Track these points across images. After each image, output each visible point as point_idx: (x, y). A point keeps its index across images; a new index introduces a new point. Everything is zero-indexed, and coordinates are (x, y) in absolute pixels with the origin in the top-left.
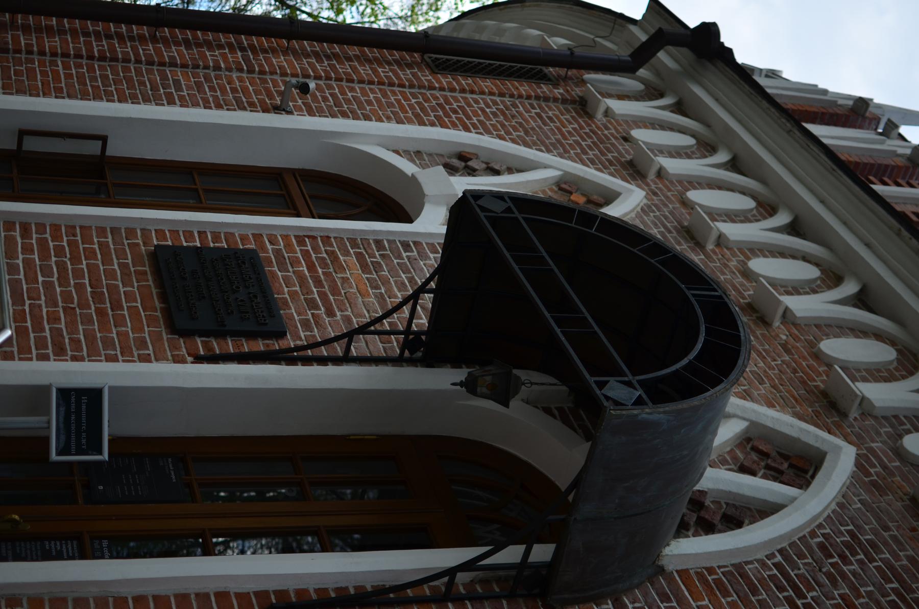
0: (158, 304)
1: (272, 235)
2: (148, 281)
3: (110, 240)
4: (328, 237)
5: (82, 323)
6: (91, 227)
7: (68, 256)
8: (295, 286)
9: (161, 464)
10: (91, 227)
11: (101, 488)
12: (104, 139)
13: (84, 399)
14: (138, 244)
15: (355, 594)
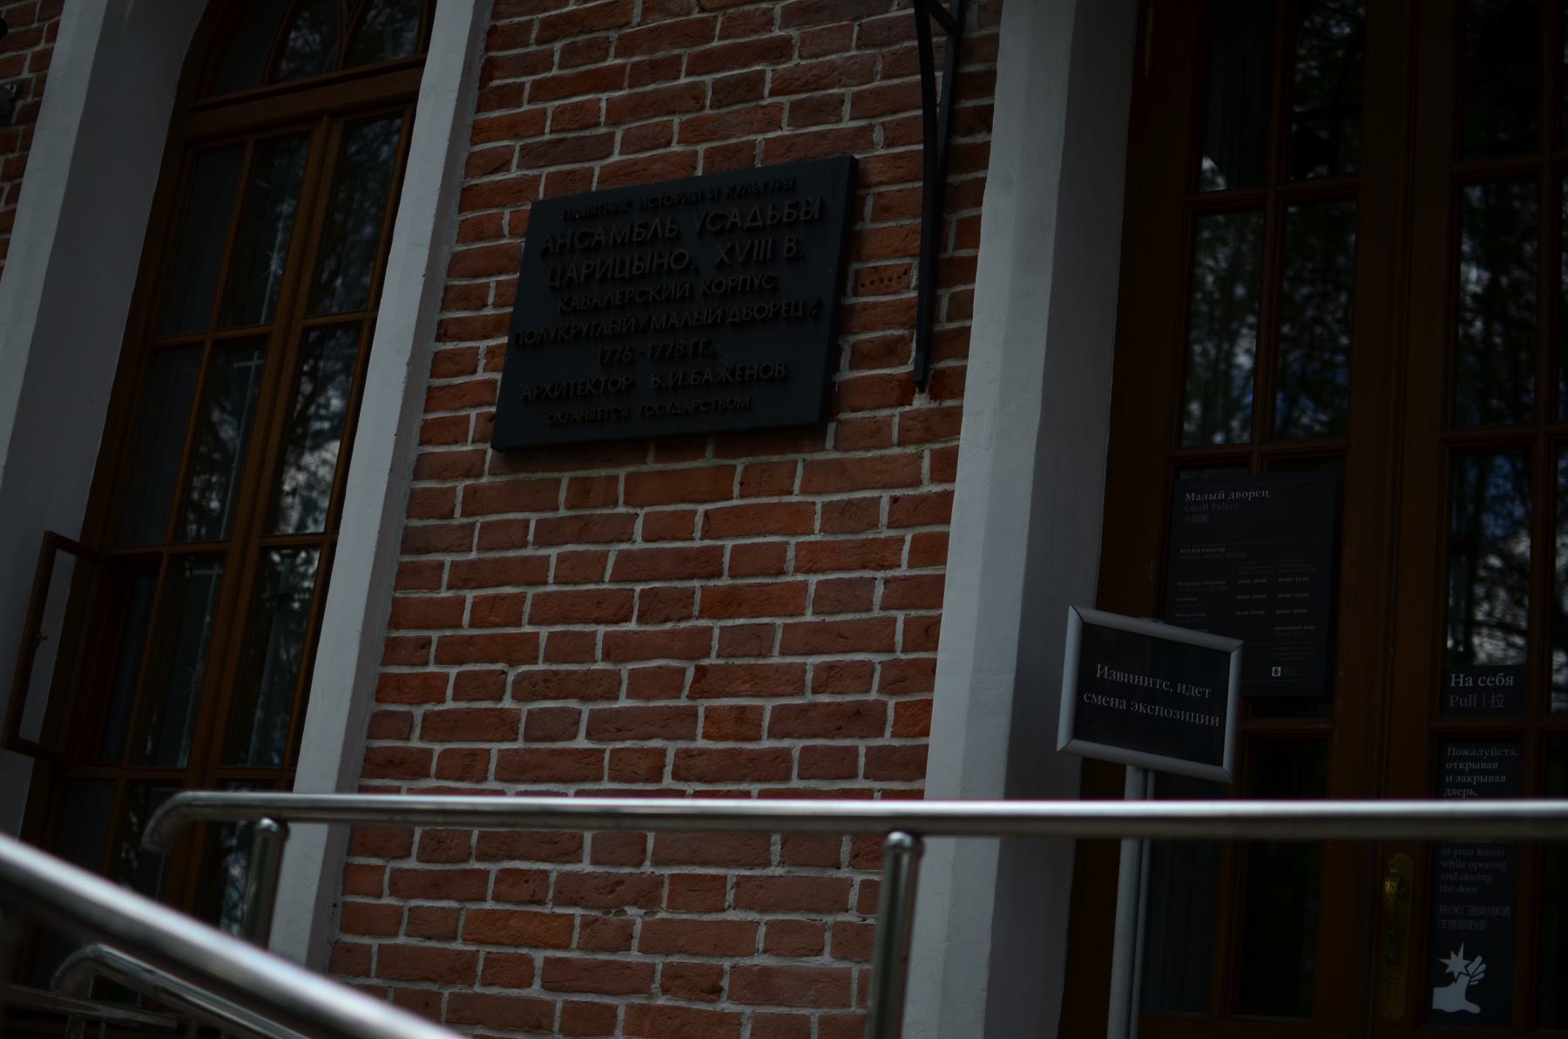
0: (708, 461)
1: (467, 164)
2: (614, 480)
3: (448, 559)
4: (493, 31)
5: (760, 655)
6: (395, 601)
7: (499, 666)
8: (668, 125)
9: (1204, 518)
10: (395, 601)
11: (1277, 671)
12: (54, 542)
13: (1103, 671)
14: (470, 493)
15: (925, 180)
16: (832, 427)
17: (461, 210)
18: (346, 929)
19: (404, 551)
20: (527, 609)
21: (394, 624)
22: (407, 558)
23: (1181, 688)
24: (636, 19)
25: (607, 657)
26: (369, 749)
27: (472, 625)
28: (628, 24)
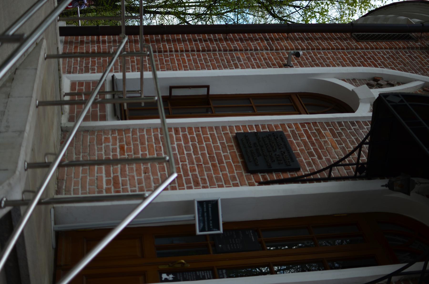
4: (316, 123)
8: (302, 146)
11: (220, 246)
12: (208, 87)
13: (210, 205)
16: (249, 174)
17: (280, 124)
18: (147, 130)
19: (215, 127)
20: (208, 143)
21: (202, 128)
22: (214, 128)
23: (211, 222)
24: (322, 140)
25: (201, 153)
26: (178, 128)
27: (204, 137)
28: (321, 139)
